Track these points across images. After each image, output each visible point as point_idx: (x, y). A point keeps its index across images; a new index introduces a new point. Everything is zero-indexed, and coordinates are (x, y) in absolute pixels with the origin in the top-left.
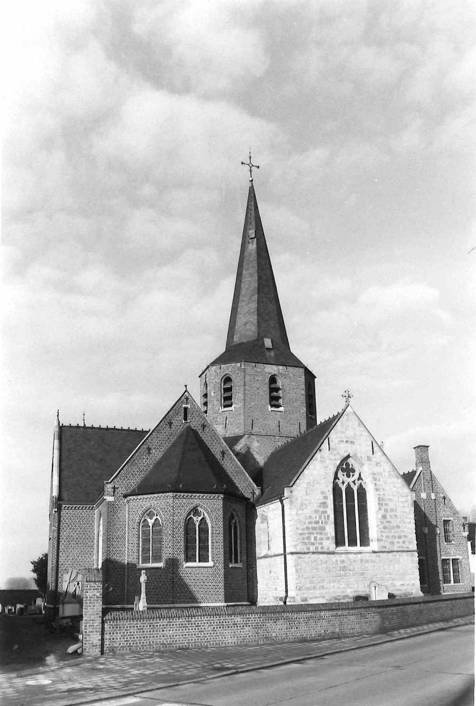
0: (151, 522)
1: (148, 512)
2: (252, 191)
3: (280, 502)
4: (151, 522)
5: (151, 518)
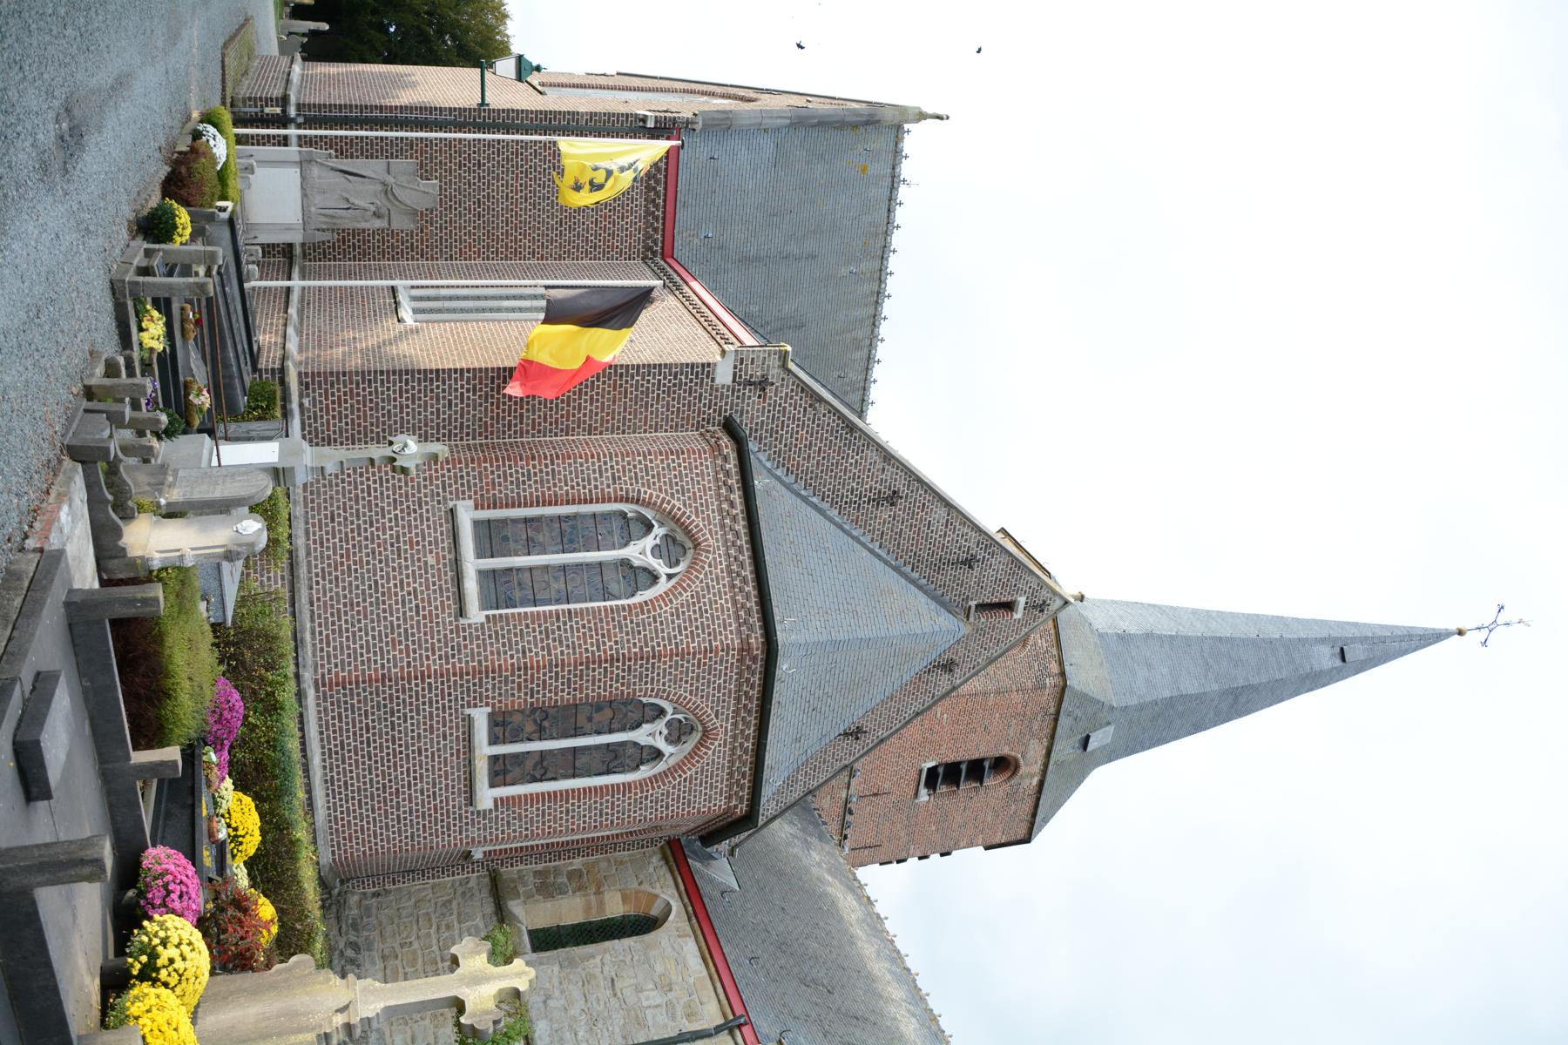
0: (640, 551)
1: (680, 536)
2: (1437, 636)
3: (721, 1021)
4: (640, 551)
5: (657, 551)
